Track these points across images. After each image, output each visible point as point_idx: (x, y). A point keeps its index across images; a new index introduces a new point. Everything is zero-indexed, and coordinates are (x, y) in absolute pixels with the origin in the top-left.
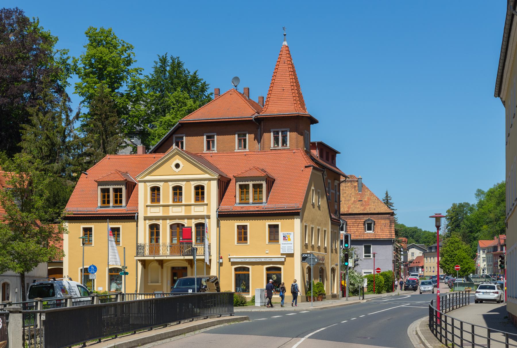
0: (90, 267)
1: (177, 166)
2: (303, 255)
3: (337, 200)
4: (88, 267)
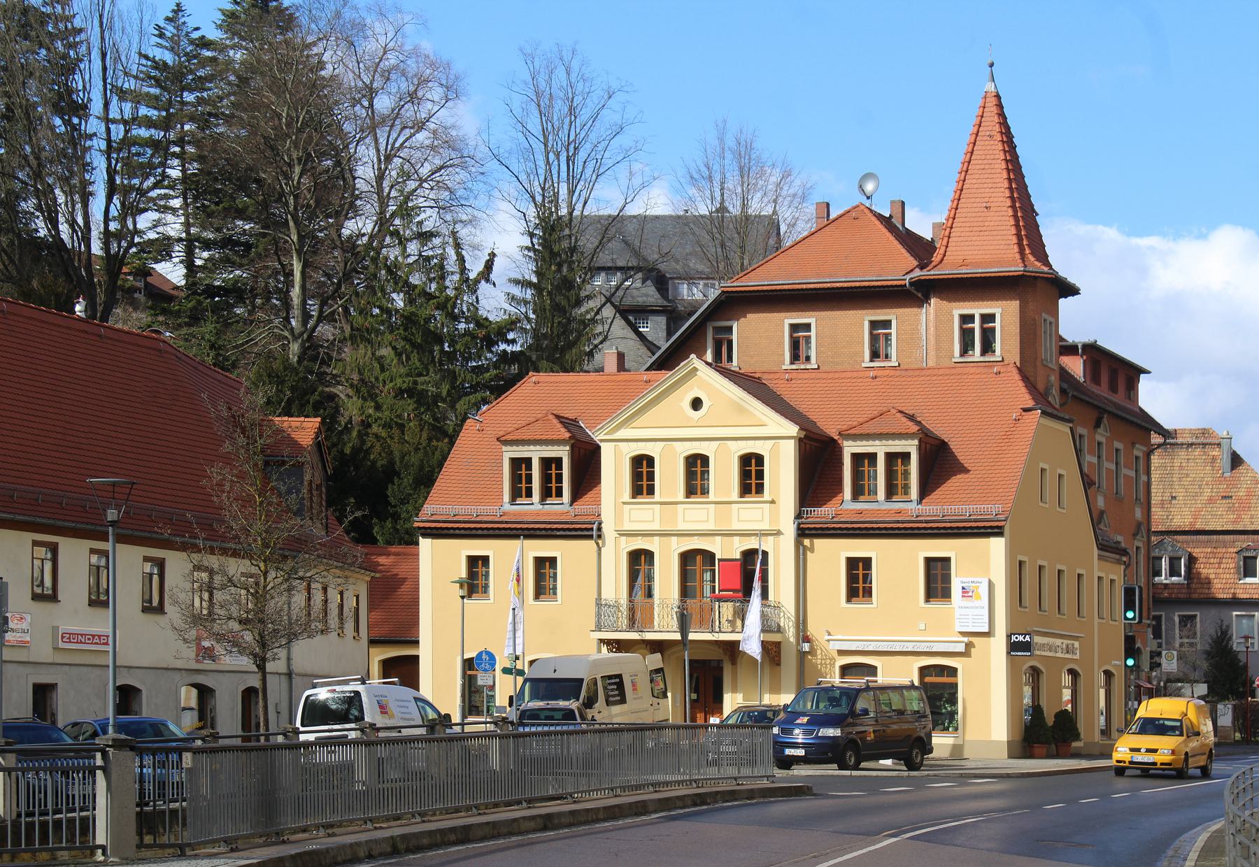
0: (480, 654)
1: (696, 404)
2: (1013, 638)
3: (1142, 496)
4: (473, 655)
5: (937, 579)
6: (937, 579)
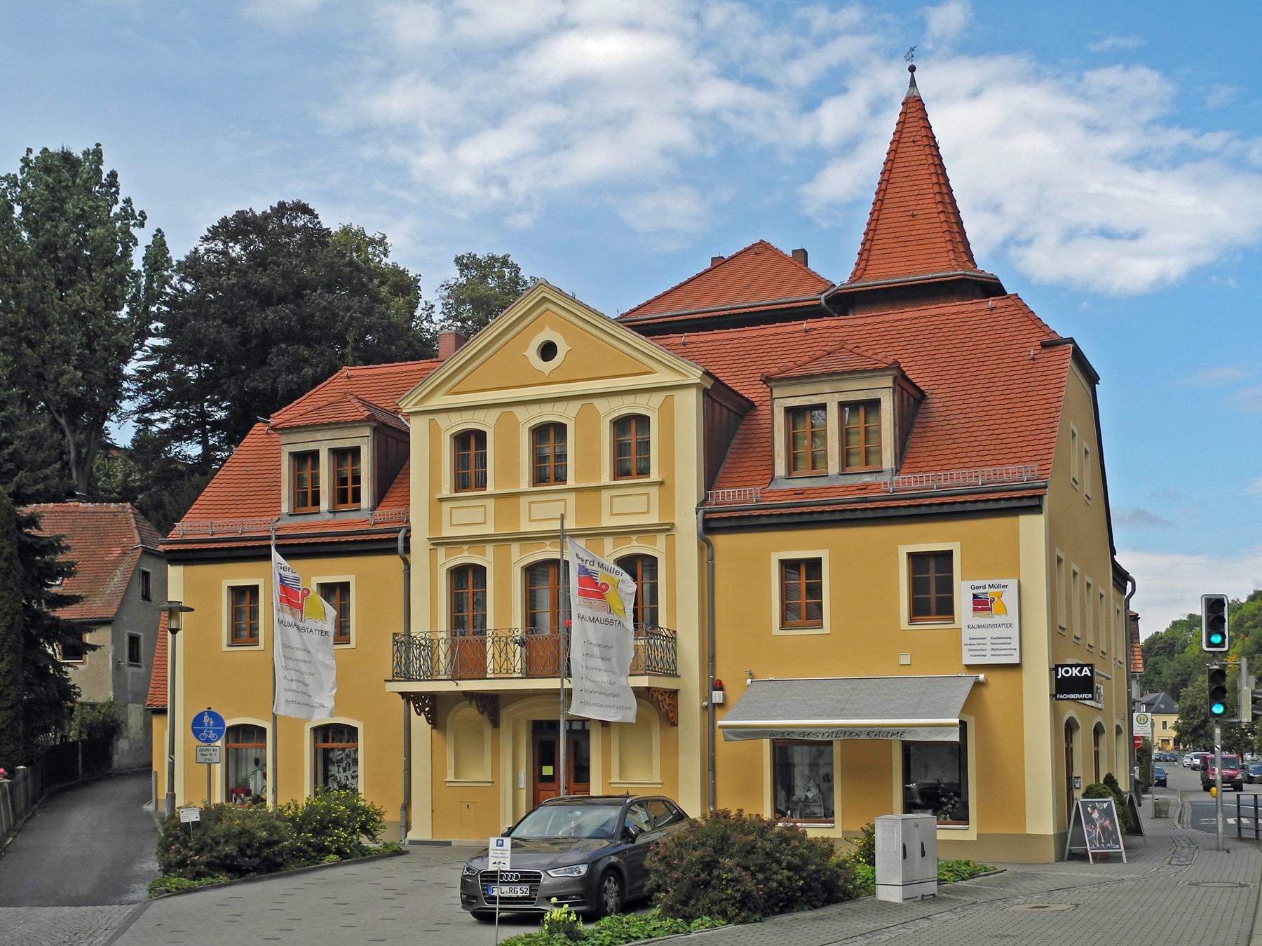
1: (548, 351)
2: (1062, 672)
5: (931, 588)
6: (931, 588)
